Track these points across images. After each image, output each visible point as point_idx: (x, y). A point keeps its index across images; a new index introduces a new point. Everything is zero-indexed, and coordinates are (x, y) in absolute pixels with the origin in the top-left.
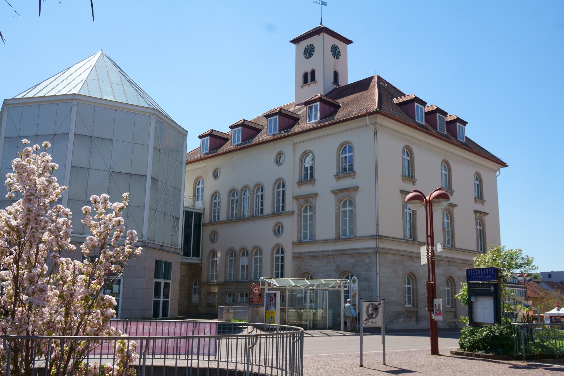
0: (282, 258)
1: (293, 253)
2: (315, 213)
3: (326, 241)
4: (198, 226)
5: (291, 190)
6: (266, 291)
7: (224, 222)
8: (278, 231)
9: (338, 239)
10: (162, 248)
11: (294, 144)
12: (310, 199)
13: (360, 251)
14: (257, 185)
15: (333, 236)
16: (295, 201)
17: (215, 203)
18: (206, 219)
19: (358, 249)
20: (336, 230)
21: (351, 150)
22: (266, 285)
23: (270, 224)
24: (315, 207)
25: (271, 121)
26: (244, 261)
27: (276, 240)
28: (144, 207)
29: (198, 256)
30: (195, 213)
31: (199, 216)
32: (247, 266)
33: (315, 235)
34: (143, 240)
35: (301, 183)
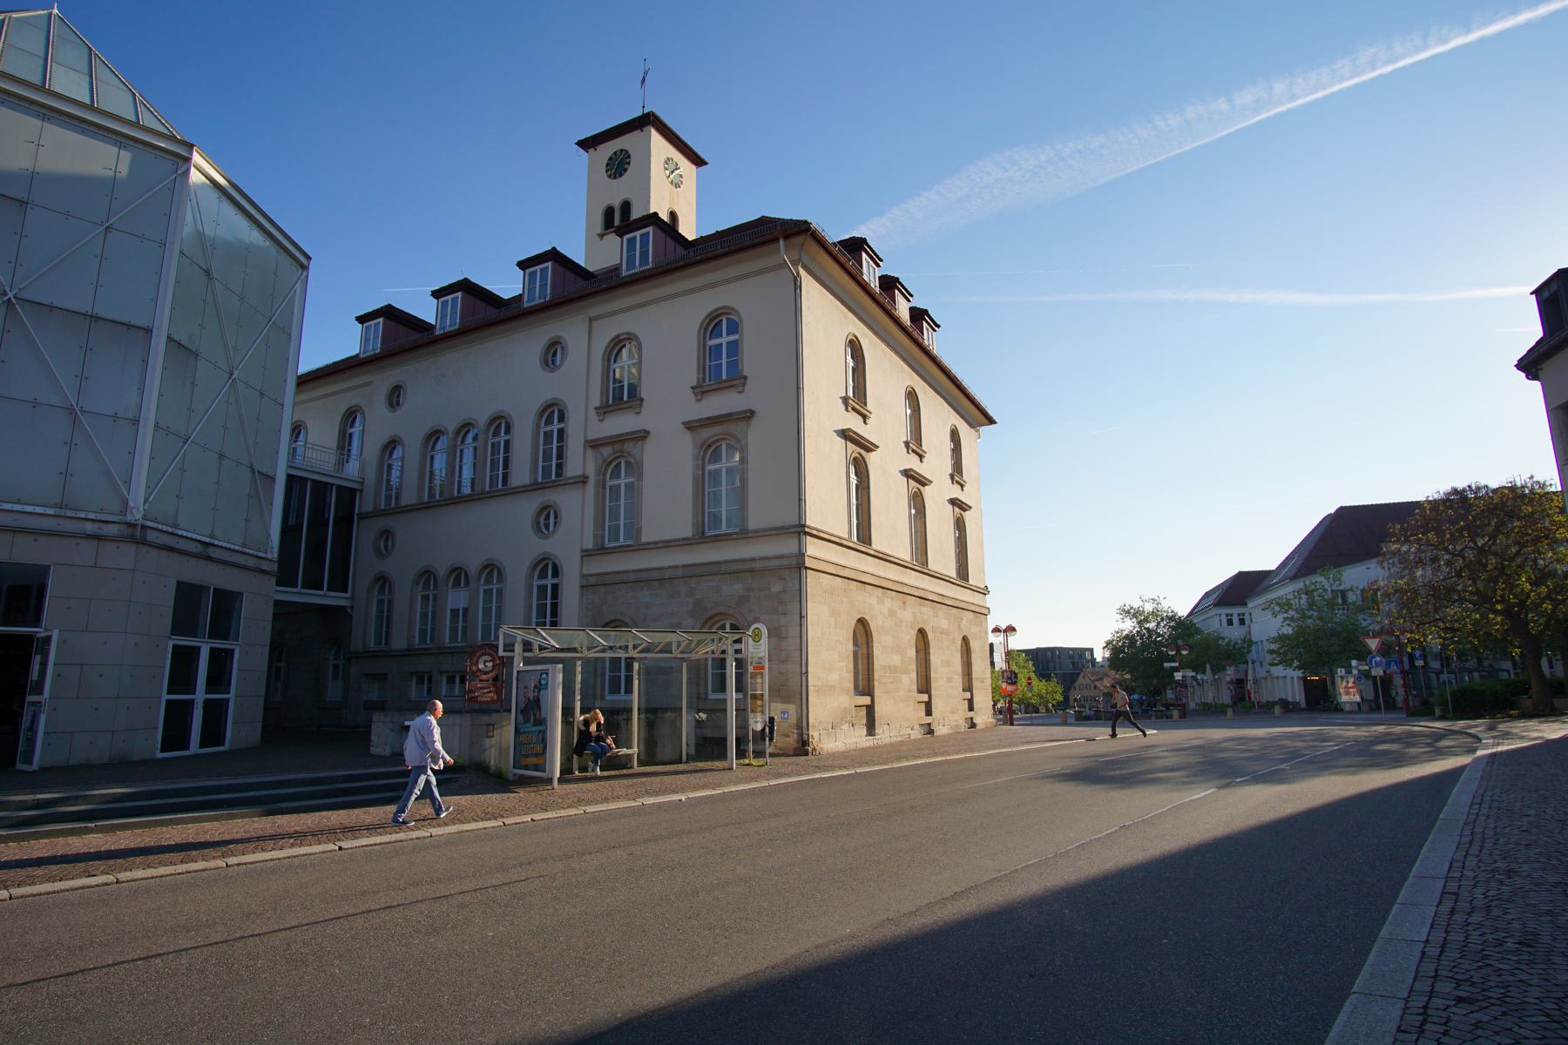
0: (555, 587)
1: (583, 576)
2: (640, 477)
3: (668, 544)
4: (346, 521)
5: (582, 425)
6: (519, 665)
7: (412, 509)
8: (547, 519)
9: (701, 537)
10: (204, 553)
11: (591, 320)
12: (628, 446)
13: (759, 565)
14: (495, 420)
15: (687, 531)
16: (589, 451)
17: (717, 473)
18: (365, 504)
19: (753, 560)
20: (695, 516)
21: (734, 328)
22: (518, 648)
23: (528, 507)
24: (640, 465)
25: (533, 275)
26: (456, 599)
27: (540, 546)
28: (136, 421)
29: (340, 583)
30: (339, 487)
31: (348, 495)
32: (465, 610)
33: (639, 531)
34: (129, 518)
35: (604, 410)
